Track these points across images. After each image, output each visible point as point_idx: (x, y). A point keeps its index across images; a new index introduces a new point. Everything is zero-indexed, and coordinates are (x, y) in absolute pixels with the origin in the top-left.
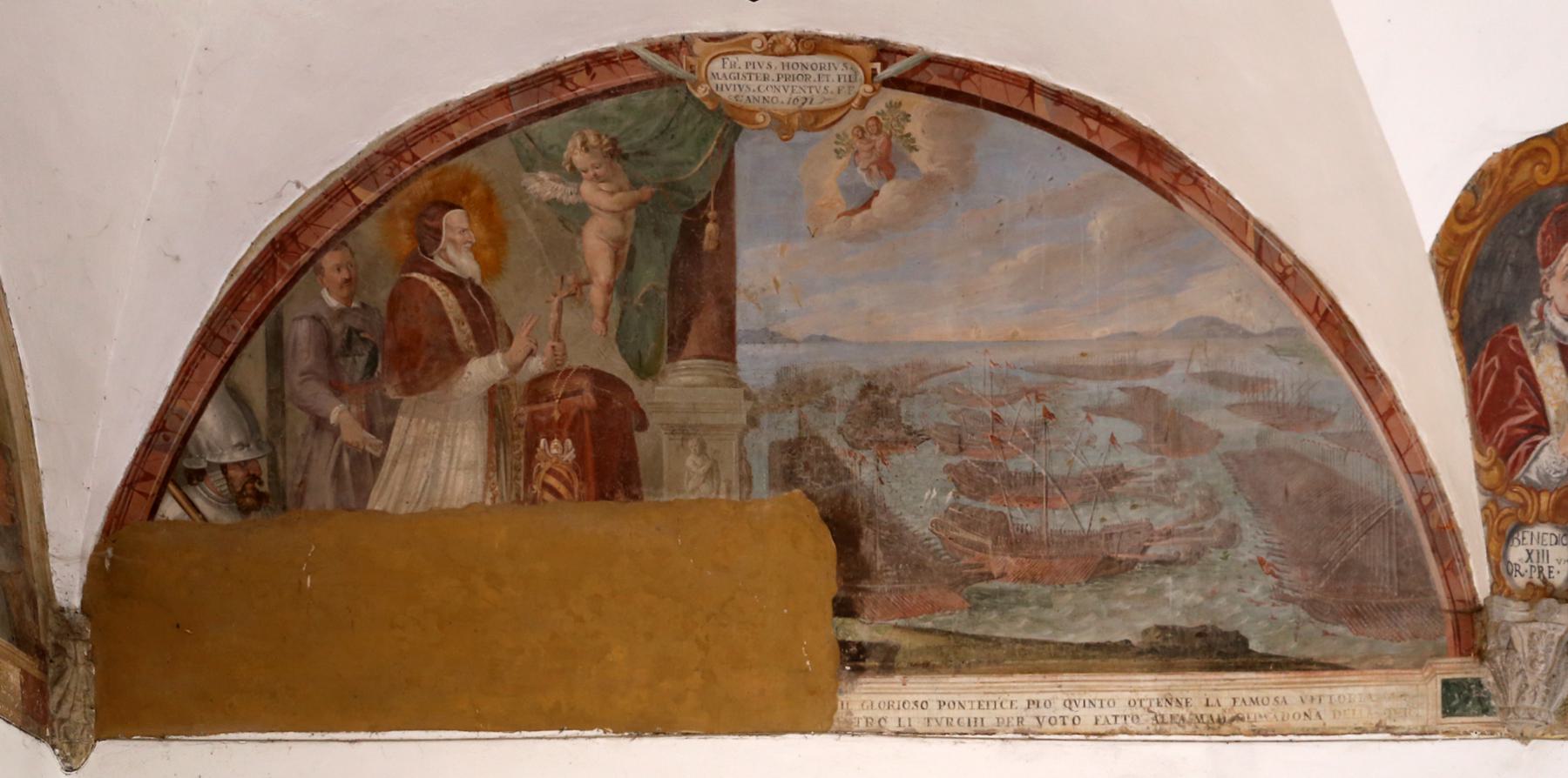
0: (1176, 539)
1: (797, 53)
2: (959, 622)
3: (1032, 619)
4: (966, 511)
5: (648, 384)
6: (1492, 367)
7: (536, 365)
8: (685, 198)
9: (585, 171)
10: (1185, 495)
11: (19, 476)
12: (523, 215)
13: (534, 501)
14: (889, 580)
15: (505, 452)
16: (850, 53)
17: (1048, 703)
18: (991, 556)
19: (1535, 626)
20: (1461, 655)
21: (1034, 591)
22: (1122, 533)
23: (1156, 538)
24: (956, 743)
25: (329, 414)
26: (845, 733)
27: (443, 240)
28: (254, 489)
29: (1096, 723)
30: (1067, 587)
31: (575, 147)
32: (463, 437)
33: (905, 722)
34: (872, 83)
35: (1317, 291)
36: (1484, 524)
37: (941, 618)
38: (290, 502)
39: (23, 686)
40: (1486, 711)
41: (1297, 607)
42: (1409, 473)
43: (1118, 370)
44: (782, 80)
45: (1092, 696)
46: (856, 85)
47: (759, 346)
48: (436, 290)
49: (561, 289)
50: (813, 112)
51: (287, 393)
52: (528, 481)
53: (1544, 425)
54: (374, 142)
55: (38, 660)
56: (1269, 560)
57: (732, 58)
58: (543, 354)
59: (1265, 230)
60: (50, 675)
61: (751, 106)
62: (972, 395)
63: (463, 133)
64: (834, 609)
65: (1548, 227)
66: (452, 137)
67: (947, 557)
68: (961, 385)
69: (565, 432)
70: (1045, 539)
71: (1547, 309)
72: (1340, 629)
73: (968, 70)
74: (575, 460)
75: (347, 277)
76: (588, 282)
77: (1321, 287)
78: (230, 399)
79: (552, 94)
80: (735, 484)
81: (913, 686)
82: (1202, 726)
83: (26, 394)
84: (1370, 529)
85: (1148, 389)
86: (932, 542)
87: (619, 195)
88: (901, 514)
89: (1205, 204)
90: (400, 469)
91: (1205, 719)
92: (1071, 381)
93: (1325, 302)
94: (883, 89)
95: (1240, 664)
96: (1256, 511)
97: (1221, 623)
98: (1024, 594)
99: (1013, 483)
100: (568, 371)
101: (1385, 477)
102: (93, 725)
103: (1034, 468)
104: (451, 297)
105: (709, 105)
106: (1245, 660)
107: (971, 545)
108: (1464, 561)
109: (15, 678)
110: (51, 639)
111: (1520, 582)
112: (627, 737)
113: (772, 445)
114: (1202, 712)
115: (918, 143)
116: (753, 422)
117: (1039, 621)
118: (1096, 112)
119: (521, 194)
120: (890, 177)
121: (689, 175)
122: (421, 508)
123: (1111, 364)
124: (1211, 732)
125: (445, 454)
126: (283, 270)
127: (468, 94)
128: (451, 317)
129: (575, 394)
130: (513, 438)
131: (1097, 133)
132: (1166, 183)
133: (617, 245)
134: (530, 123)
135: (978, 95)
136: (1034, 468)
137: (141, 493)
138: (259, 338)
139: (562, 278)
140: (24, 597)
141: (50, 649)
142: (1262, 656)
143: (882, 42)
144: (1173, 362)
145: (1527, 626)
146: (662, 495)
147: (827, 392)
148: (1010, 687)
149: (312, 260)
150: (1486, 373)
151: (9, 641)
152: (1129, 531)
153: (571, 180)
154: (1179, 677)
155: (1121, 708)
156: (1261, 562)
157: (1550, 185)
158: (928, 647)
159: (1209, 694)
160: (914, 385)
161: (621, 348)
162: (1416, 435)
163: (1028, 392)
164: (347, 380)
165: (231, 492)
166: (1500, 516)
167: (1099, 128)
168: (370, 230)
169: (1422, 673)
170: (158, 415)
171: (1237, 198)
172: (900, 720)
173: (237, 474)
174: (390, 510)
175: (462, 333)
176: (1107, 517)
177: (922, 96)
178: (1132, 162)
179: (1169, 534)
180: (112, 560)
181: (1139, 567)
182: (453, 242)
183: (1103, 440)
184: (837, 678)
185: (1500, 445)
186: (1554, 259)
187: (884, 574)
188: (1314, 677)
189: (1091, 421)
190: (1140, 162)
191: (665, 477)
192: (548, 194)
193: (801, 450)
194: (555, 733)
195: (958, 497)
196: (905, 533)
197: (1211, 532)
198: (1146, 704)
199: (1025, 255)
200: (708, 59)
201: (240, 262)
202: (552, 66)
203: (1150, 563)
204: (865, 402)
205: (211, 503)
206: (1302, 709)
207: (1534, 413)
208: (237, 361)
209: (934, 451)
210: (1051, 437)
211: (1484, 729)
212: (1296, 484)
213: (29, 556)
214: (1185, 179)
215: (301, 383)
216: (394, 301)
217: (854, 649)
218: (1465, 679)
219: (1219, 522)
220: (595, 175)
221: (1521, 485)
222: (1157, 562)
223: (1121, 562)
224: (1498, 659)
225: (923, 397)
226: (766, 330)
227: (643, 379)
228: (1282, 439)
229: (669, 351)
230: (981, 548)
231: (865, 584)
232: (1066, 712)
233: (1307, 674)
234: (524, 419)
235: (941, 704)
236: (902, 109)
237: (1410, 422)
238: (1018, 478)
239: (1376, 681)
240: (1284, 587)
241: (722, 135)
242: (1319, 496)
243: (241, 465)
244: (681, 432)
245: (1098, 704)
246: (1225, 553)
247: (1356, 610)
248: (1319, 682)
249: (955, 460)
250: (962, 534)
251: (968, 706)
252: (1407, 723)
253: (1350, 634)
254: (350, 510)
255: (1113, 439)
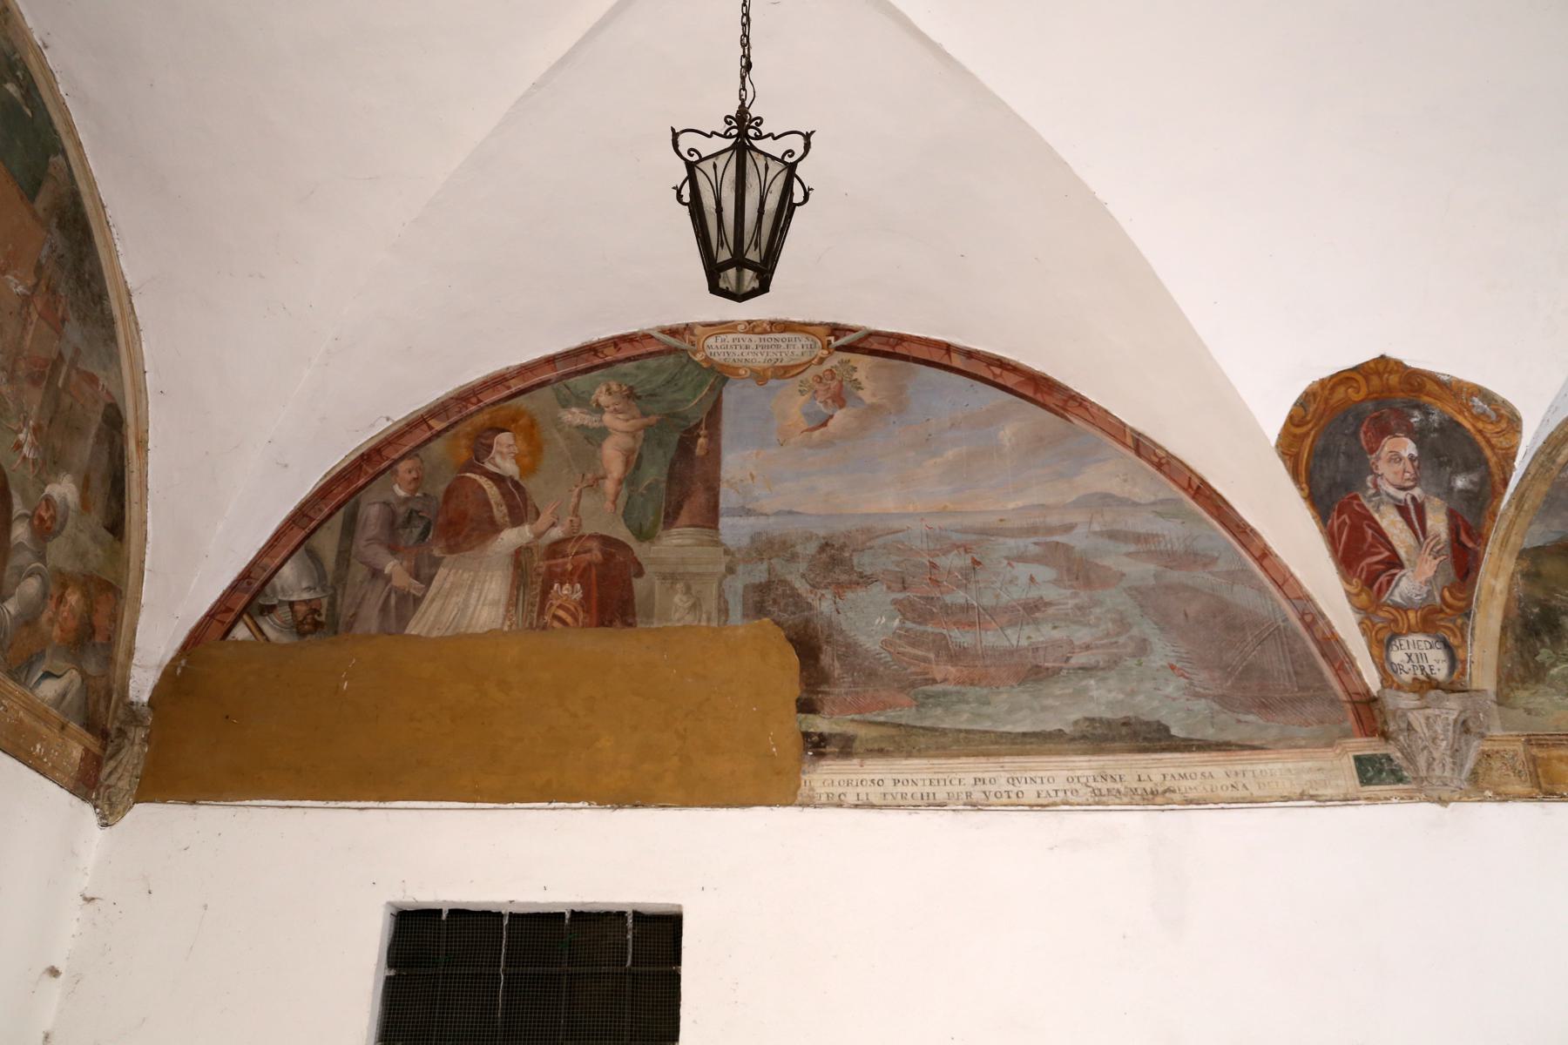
0: (1094, 651)
1: (771, 332)
2: (908, 716)
3: (972, 713)
4: (911, 632)
5: (646, 545)
6: (1344, 522)
7: (557, 533)
8: (683, 423)
9: (608, 407)
10: (1099, 619)
11: (123, 609)
12: (557, 436)
13: (544, 628)
14: (845, 685)
15: (524, 593)
16: (811, 331)
17: (992, 780)
18: (934, 666)
19: (1428, 711)
20: (1367, 736)
21: (972, 692)
22: (1046, 647)
23: (1077, 650)
24: (910, 814)
25: (385, 567)
26: (808, 806)
27: (493, 451)
28: (313, 619)
29: (1039, 797)
30: (1001, 689)
31: (601, 392)
32: (491, 582)
33: (863, 797)
34: (828, 349)
35: (1189, 474)
36: (1363, 635)
37: (893, 714)
38: (341, 628)
39: (82, 760)
40: (1401, 780)
41: (1209, 701)
42: (1289, 599)
43: (1032, 531)
44: (760, 349)
45: (1033, 774)
46: (816, 351)
47: (737, 518)
48: (483, 484)
49: (582, 481)
50: (783, 367)
51: (353, 552)
52: (541, 613)
53: (1397, 561)
54: (450, 392)
55: (101, 740)
56: (1178, 665)
57: (723, 336)
58: (563, 525)
59: (1139, 434)
60: (108, 752)
61: (735, 365)
62: (911, 549)
63: (516, 385)
64: (797, 707)
65: (1367, 428)
66: (509, 388)
67: (896, 667)
68: (903, 544)
69: (575, 578)
70: (980, 652)
71: (1379, 481)
72: (1251, 718)
73: (900, 339)
74: (583, 598)
75: (415, 476)
76: (604, 478)
77: (1191, 471)
78: (306, 557)
79: (587, 361)
80: (714, 614)
81: (870, 767)
82: (1137, 798)
83: (145, 553)
84: (1263, 640)
85: (1058, 543)
86: (883, 655)
87: (632, 422)
88: (855, 635)
89: (1090, 418)
90: (436, 605)
91: (1139, 792)
92: (993, 538)
93: (1196, 482)
94: (837, 352)
95: (1164, 747)
96: (1162, 629)
97: (1143, 715)
98: (964, 694)
99: (950, 612)
100: (581, 537)
101: (1269, 602)
102: (134, 792)
103: (967, 601)
104: (495, 488)
105: (705, 365)
106: (1168, 743)
107: (916, 658)
108: (1352, 663)
109: (77, 753)
110: (117, 724)
111: (1406, 678)
112: (609, 808)
113: (746, 587)
114: (1136, 786)
115: (863, 385)
116: (731, 570)
117: (979, 715)
118: (998, 363)
119: (557, 423)
120: (841, 407)
121: (687, 408)
122: (449, 633)
123: (1025, 526)
124: (1146, 802)
125: (475, 595)
126: (366, 473)
127: (524, 361)
128: (492, 502)
129: (585, 552)
130: (532, 583)
131: (1001, 375)
132: (1057, 406)
133: (628, 455)
134: (569, 378)
135: (908, 354)
136: (967, 601)
137: (219, 621)
138: (339, 516)
139: (583, 475)
140: (102, 693)
141: (113, 733)
142: (1184, 740)
143: (834, 324)
144: (1076, 524)
145: (1421, 711)
146: (652, 623)
147: (792, 549)
148: (957, 768)
149: (390, 466)
150: (1339, 527)
151: (80, 726)
152: (1052, 645)
153: (596, 412)
154: (1110, 757)
155: (1061, 784)
156: (1172, 667)
157: (1362, 401)
158: (881, 736)
159: (1140, 771)
160: (863, 543)
161: (625, 520)
162: (1289, 572)
163: (958, 547)
164: (403, 543)
165: (294, 621)
166: (1376, 629)
167: (1001, 373)
168: (438, 447)
169: (1334, 751)
170: (246, 567)
171: (1115, 414)
172: (858, 795)
173: (301, 609)
174: (423, 634)
175: (500, 512)
176: (1032, 636)
177: (865, 356)
178: (1030, 393)
179: (1088, 647)
180: (184, 669)
181: (1064, 672)
182: (501, 453)
183: (1024, 580)
184: (801, 761)
185: (1363, 577)
186: (1377, 449)
187: (841, 680)
188: (1235, 756)
189: (1013, 567)
190: (1035, 393)
191: (656, 610)
192: (578, 421)
193: (770, 590)
194: (545, 805)
195: (904, 623)
196: (859, 649)
197: (1125, 646)
198: (1083, 780)
199: (950, 454)
200: (705, 337)
201: (334, 468)
202: (589, 343)
203: (1074, 669)
204: (824, 556)
205: (275, 629)
206: (1228, 782)
207: (1387, 554)
208: (318, 532)
209: (882, 590)
210: (979, 578)
211: (1403, 795)
212: (1194, 608)
213: (116, 665)
214: (1071, 403)
215: (365, 546)
216: (449, 492)
217: (815, 738)
218: (1376, 755)
219: (1131, 638)
220: (615, 409)
221: (1389, 606)
222: (1080, 668)
223: (1047, 669)
224: (1401, 738)
225: (872, 551)
226: (743, 507)
227: (642, 541)
228: (1175, 576)
229: (664, 522)
230: (925, 660)
231: (824, 688)
232: (1010, 788)
233: (1229, 753)
234: (543, 570)
235: (896, 782)
236: (851, 364)
237: (1282, 561)
238: (954, 608)
239: (1292, 758)
240: (1195, 686)
241: (714, 382)
242: (1215, 617)
243: (306, 602)
244: (671, 578)
245: (1039, 781)
246: (1139, 661)
247: (1263, 703)
248: (1240, 760)
249: (900, 596)
250: (909, 650)
251: (920, 783)
252: (1329, 792)
253: (1261, 721)
254: (389, 634)
255: (1032, 579)
